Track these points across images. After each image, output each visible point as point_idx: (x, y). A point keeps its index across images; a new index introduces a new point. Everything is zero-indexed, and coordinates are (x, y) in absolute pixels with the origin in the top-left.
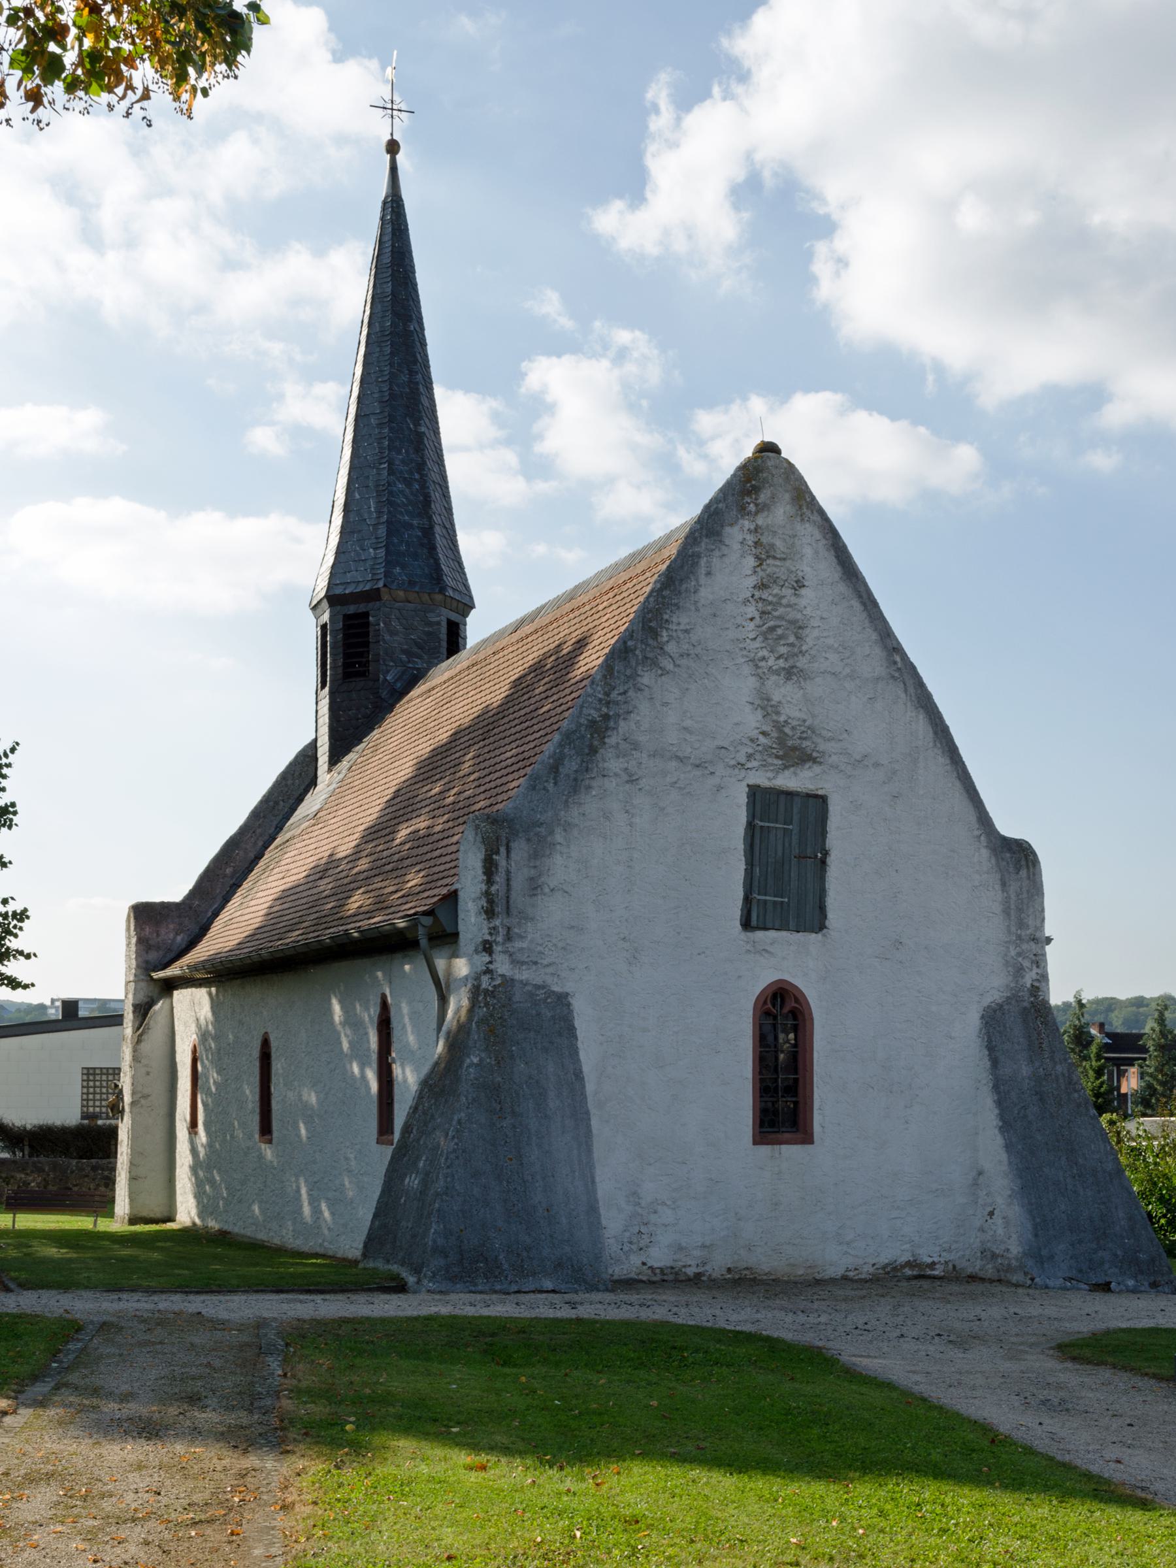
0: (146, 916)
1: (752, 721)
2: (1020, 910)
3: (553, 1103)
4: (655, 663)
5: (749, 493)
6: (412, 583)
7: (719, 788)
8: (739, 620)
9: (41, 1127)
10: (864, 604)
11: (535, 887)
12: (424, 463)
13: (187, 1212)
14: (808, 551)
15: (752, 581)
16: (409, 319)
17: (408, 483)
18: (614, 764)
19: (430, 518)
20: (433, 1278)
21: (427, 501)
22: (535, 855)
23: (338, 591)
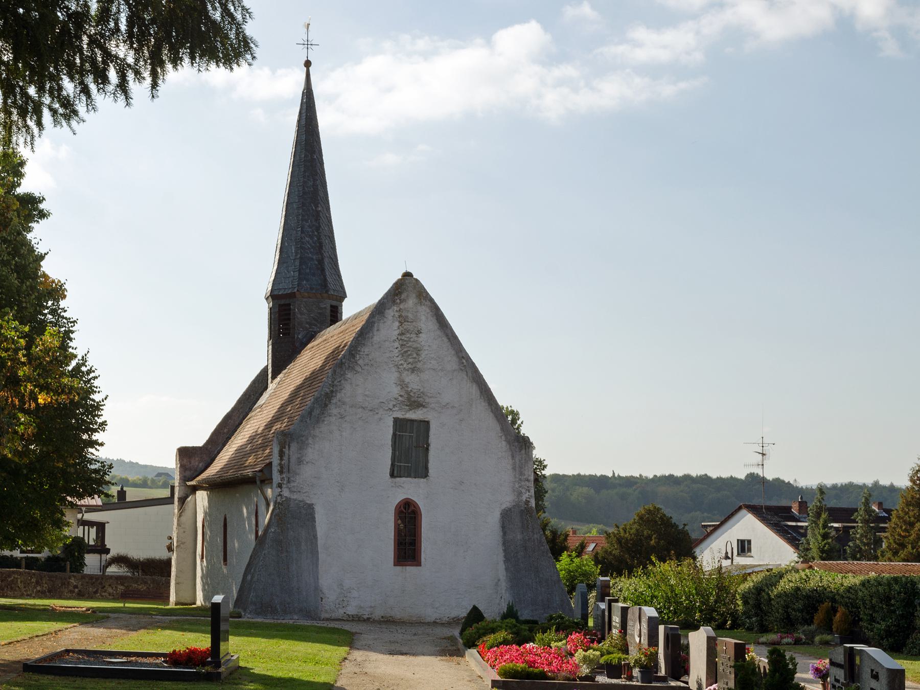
0: (185, 453)
1: (396, 391)
2: (521, 468)
4: (353, 369)
5: (397, 295)
6: (312, 289)
7: (380, 419)
8: (391, 349)
11: (300, 461)
12: (320, 226)
13: (200, 601)
14: (423, 318)
15: (397, 332)
16: (314, 152)
17: (311, 237)
18: (334, 411)
19: (322, 254)
20: (250, 613)
22: (301, 449)
23: (276, 293)
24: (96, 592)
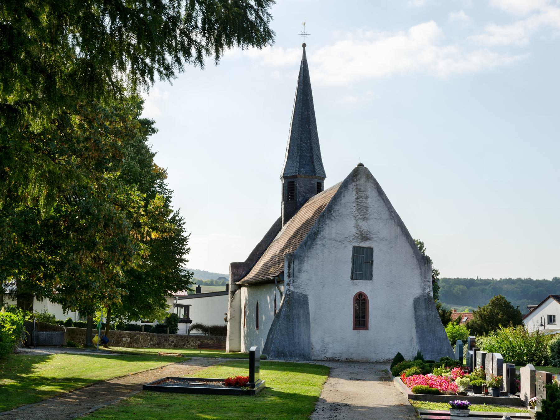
0: (235, 266)
2: (425, 274)
3: (302, 319)
4: (330, 218)
5: (355, 176)
7: (345, 247)
9: (214, 326)
10: (384, 201)
11: (300, 271)
14: (370, 189)
15: (355, 197)
16: (308, 95)
17: (306, 143)
18: (319, 242)
19: (312, 153)
20: (271, 357)
21: (312, 149)
22: (300, 263)
23: (286, 175)
24: (184, 345)
